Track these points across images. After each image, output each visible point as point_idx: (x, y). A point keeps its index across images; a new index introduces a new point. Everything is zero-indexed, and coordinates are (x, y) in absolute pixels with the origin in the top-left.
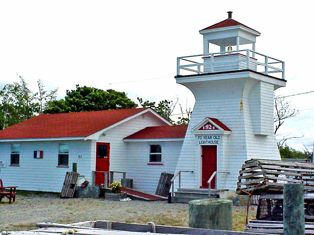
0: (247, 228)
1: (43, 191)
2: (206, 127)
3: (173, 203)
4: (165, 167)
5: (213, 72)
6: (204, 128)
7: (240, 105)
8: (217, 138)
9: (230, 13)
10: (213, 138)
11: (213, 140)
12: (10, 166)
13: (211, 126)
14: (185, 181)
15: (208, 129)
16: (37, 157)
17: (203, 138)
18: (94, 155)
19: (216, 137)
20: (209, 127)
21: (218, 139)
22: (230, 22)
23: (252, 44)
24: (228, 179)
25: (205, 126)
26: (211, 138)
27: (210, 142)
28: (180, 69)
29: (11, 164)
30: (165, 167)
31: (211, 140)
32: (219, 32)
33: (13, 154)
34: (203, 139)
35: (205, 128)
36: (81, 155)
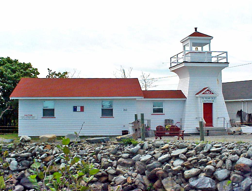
0: (78, 156)
1: (85, 135)
2: (206, 92)
3: (210, 136)
4: (166, 116)
5: (206, 62)
6: (205, 93)
7: (217, 81)
8: (213, 99)
9: (196, 29)
10: (211, 98)
11: (211, 100)
12: (42, 118)
13: (209, 92)
14: (222, 123)
15: (208, 94)
16: (77, 111)
17: (205, 98)
18: (201, 106)
19: (213, 98)
20: (208, 92)
21: (214, 99)
22: (196, 34)
23: (201, 47)
24: (218, 121)
25: (206, 92)
26: (210, 98)
27: (209, 101)
28: (226, 59)
29: (102, 116)
30: (166, 116)
31: (209, 100)
32: (192, 39)
33: (44, 108)
34: (205, 99)
35: (206, 93)
36: (127, 109)
